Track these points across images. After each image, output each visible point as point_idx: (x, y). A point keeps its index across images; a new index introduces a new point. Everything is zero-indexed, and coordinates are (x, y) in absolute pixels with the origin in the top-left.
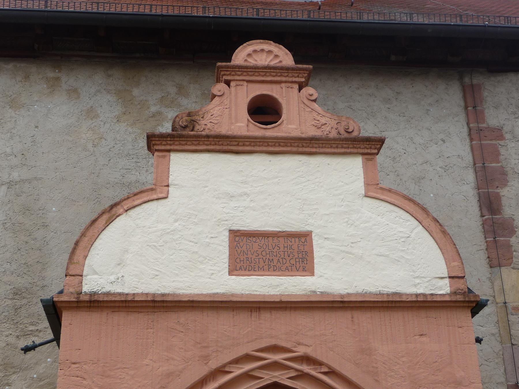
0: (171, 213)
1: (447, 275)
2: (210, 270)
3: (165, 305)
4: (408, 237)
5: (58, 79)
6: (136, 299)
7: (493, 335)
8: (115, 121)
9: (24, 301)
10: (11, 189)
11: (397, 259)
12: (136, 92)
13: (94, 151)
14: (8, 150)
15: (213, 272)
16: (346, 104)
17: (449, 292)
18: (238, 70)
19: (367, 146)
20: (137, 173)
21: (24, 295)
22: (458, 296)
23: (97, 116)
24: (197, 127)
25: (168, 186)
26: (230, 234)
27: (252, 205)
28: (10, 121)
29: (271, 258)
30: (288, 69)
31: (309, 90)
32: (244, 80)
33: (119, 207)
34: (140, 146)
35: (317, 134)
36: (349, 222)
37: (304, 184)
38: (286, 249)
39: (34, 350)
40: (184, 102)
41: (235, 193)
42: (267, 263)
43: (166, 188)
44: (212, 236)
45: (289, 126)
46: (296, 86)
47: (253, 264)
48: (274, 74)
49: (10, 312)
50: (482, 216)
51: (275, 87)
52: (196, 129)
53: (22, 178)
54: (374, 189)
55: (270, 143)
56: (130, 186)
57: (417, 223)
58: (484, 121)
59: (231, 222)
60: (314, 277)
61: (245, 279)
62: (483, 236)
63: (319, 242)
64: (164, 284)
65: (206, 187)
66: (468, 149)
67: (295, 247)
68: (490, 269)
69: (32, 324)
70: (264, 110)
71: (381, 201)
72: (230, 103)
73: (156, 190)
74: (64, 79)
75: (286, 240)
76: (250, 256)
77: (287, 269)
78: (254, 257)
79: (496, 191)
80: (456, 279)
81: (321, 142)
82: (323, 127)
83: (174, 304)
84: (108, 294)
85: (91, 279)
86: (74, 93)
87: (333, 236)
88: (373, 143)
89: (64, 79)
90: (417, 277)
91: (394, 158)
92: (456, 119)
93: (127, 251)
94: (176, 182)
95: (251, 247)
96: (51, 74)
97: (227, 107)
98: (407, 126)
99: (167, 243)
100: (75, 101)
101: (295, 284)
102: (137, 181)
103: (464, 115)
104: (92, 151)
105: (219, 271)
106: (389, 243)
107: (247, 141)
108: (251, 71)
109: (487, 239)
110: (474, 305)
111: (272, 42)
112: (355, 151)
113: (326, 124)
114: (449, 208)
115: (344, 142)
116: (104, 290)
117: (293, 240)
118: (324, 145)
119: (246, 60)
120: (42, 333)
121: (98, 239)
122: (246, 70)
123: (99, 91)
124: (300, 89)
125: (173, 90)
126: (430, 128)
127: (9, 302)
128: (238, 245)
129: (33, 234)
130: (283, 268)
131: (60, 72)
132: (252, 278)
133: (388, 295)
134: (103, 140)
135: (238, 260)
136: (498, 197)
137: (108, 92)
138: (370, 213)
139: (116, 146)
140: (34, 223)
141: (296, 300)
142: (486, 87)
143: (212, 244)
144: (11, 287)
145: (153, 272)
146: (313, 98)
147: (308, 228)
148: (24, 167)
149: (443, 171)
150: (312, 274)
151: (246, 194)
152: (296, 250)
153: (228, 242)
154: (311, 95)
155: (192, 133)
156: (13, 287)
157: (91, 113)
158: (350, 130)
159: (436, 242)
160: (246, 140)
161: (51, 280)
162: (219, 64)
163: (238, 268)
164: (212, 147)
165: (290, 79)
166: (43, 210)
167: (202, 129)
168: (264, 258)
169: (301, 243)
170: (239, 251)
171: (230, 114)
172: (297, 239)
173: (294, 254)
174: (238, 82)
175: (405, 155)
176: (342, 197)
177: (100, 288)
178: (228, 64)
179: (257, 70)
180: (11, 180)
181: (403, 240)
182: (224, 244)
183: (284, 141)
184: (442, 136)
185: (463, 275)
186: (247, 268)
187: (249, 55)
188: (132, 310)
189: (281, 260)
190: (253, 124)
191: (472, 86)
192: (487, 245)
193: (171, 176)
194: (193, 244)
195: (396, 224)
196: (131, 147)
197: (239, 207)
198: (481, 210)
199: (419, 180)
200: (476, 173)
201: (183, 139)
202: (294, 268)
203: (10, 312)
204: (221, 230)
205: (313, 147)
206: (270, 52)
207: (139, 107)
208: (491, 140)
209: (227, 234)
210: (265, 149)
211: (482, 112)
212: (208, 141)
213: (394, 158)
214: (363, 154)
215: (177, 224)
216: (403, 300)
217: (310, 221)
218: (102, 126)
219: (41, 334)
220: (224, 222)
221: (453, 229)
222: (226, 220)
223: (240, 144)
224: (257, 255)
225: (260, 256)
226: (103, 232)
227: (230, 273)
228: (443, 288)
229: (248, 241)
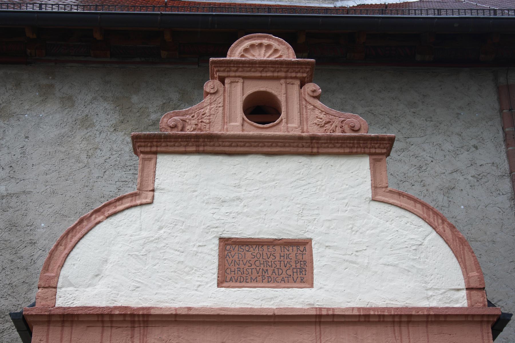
0: (156, 220)
2: (197, 281)
4: (420, 245)
8: (112, 130)
11: (407, 268)
12: (135, 99)
13: (88, 163)
15: (201, 284)
16: (367, 109)
21: (7, 318)
23: (92, 125)
25: (153, 190)
26: (220, 242)
27: (246, 210)
29: (265, 268)
30: (289, 64)
31: (310, 87)
32: (239, 77)
36: (353, 229)
37: (304, 188)
38: (282, 258)
41: (227, 198)
42: (260, 274)
43: (151, 193)
44: (200, 244)
46: (298, 82)
53: (9, 192)
55: (266, 144)
57: (430, 229)
59: (221, 229)
60: (313, 289)
61: (235, 291)
63: (319, 251)
64: (146, 296)
65: (195, 191)
66: (504, 156)
67: (293, 256)
70: (262, 109)
71: (390, 205)
72: (224, 101)
73: (140, 195)
75: (283, 249)
76: (242, 266)
77: (283, 280)
82: (326, 126)
85: (65, 291)
86: (68, 101)
87: (335, 244)
90: (430, 289)
91: (420, 167)
92: (490, 123)
93: (106, 261)
94: (162, 187)
95: (243, 257)
96: (44, 82)
97: (220, 105)
98: (435, 131)
99: (150, 252)
100: (69, 109)
101: (291, 297)
103: (499, 119)
104: (86, 163)
105: (207, 283)
106: (398, 252)
107: (241, 142)
110: (495, 320)
113: (330, 122)
117: (291, 248)
121: (76, 248)
123: (95, 99)
124: (302, 85)
126: (460, 133)
129: (19, 252)
132: (243, 290)
137: (105, 99)
138: (377, 219)
139: (112, 157)
140: (21, 240)
141: (291, 314)
143: (200, 253)
145: (133, 284)
146: (315, 94)
147: (308, 236)
148: (12, 180)
149: (476, 181)
150: (312, 286)
151: (238, 199)
152: (294, 259)
153: (218, 251)
154: (314, 91)
157: (86, 122)
158: (356, 128)
162: (211, 59)
163: (228, 279)
166: (31, 226)
168: (258, 269)
169: (299, 252)
170: (230, 261)
171: (224, 113)
172: (295, 248)
173: (292, 263)
174: (233, 79)
175: (433, 163)
176: (346, 201)
181: (414, 248)
182: (213, 253)
183: (283, 141)
184: (474, 142)
185: (482, 287)
186: (239, 279)
187: (246, 50)
189: (276, 271)
190: (248, 123)
194: (178, 253)
195: (409, 229)
196: (128, 158)
197: (231, 213)
199: (448, 190)
202: (291, 279)
204: (210, 237)
207: (138, 114)
209: (217, 242)
213: (420, 167)
214: (370, 154)
215: (162, 232)
217: (310, 227)
218: (98, 135)
220: (213, 229)
221: (487, 244)
222: (217, 227)
223: (233, 144)
224: (250, 265)
227: (220, 284)
228: (460, 301)
229: (240, 250)
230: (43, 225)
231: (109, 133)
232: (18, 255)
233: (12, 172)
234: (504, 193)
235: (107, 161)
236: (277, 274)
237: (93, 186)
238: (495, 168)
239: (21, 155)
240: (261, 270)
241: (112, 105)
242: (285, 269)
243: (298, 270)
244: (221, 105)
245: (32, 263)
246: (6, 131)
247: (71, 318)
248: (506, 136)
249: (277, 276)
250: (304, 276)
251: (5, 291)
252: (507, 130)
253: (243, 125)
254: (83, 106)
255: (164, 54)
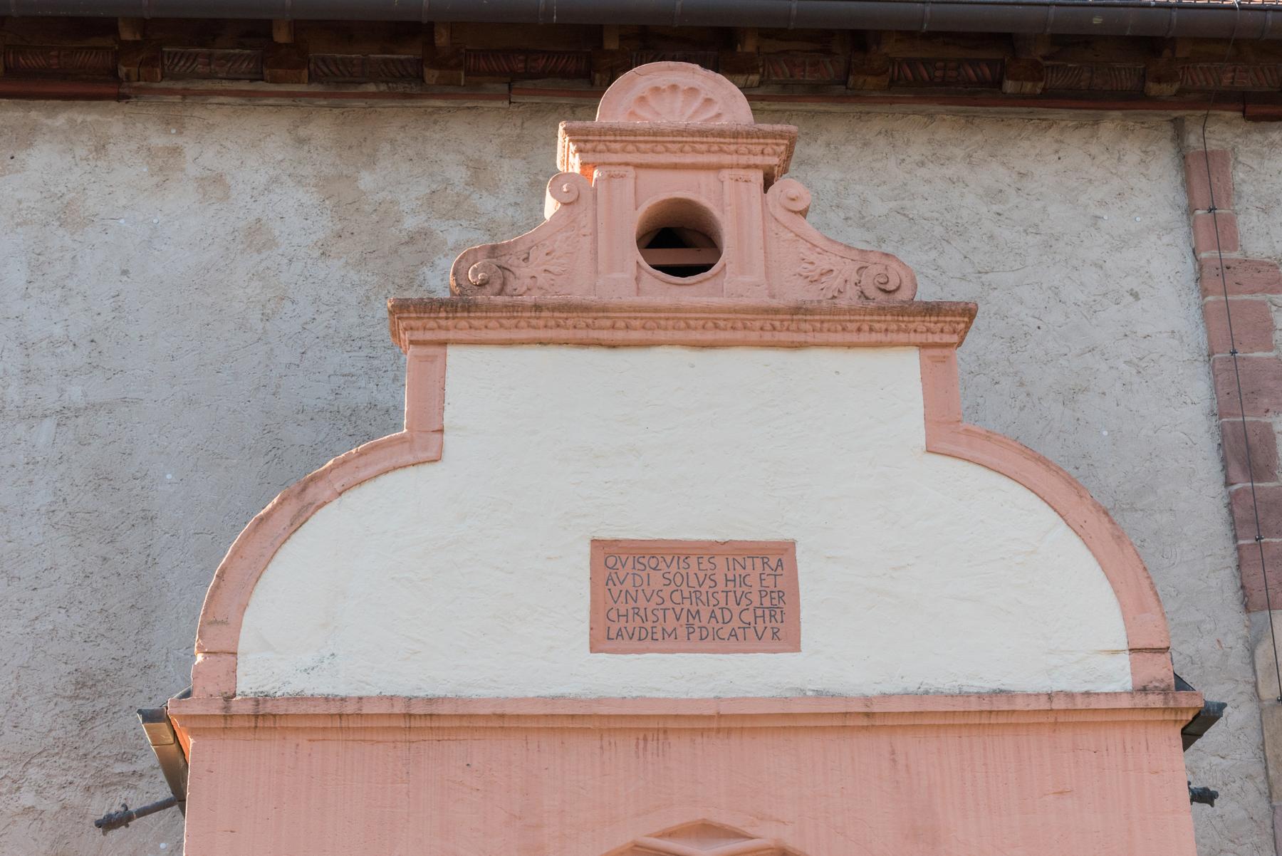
1: (1125, 647)
3: (435, 724)
5: (176, 151)
6: (364, 712)
7: (1249, 777)
8: (317, 253)
9: (101, 704)
10: (65, 429)
12: (367, 180)
13: (265, 331)
14: (58, 331)
16: (893, 204)
17: (1129, 687)
18: (612, 138)
19: (932, 325)
20: (371, 385)
21: (100, 688)
22: (1151, 697)
24: (512, 284)
28: (61, 259)
29: (694, 609)
32: (627, 164)
33: (321, 484)
34: (378, 316)
35: (808, 297)
39: (127, 826)
40: (486, 203)
42: (683, 620)
43: (437, 435)
45: (738, 277)
47: (648, 625)
48: (704, 147)
49: (69, 728)
50: (1228, 483)
51: (704, 178)
52: (509, 289)
54: (950, 431)
56: (353, 418)
58: (1234, 244)
62: (1230, 535)
67: (753, 580)
68: (1244, 617)
69: (123, 758)
71: (966, 463)
74: (191, 150)
76: (642, 602)
78: (652, 605)
79: (1263, 420)
80: (1148, 655)
81: (817, 317)
82: (824, 279)
83: (456, 723)
84: (298, 698)
88: (948, 319)
89: (191, 150)
92: (1166, 239)
95: (646, 583)
96: (158, 140)
102: (372, 406)
103: (1186, 229)
108: (646, 142)
109: (1241, 542)
111: (697, 66)
112: (902, 337)
114: (1147, 464)
115: (876, 318)
116: (290, 689)
118: (826, 325)
119: (632, 113)
120: (145, 780)
122: (632, 138)
125: (458, 175)
127: (67, 705)
128: (614, 576)
129: (119, 538)
130: (725, 633)
131: (180, 133)
133: (980, 695)
134: (288, 304)
135: (613, 615)
136: (1268, 436)
137: (300, 181)
140: (122, 512)
142: (1240, 158)
144: (71, 668)
146: (800, 206)
149: (1134, 372)
150: (796, 648)
152: (757, 587)
155: (499, 300)
156: (74, 667)
158: (890, 287)
159: (1100, 564)
160: (633, 315)
161: (165, 651)
163: (613, 634)
164: (550, 334)
165: (743, 160)
167: (525, 288)
169: (768, 571)
175: (1040, 332)
177: (277, 685)
178: (588, 123)
179: (659, 139)
180: (66, 405)
183: (726, 316)
185: (1163, 645)
188: (357, 737)
189: (718, 613)
191: (1206, 155)
192: (1240, 558)
193: (447, 408)
196: (355, 320)
198: (1225, 468)
200: (1216, 376)
201: (479, 314)
203: (69, 728)
205: (798, 330)
206: (693, 91)
207: (375, 217)
208: (1253, 292)
209: (587, 549)
210: (679, 335)
211: (1231, 221)
212: (538, 318)
214: (922, 346)
216: (1018, 708)
219: (142, 784)
224: (660, 601)
225: (668, 604)
226: (285, 546)
228: (1116, 676)
230: (169, 476)
231: (310, 262)
232: (118, 545)
233: (95, 354)
234: (1196, 400)
235: (307, 327)
236: (720, 620)
237: (278, 386)
238: (1176, 342)
239: (114, 314)
240: (685, 612)
241: (316, 195)
242: (736, 610)
243: (767, 612)
244: (587, 230)
245: (149, 564)
246: (78, 257)
247: (265, 718)
248: (1201, 268)
249: (720, 625)
250: (779, 625)
251: (92, 626)
252: (1203, 255)
253: (637, 279)
254: (248, 199)
255: (431, 75)
